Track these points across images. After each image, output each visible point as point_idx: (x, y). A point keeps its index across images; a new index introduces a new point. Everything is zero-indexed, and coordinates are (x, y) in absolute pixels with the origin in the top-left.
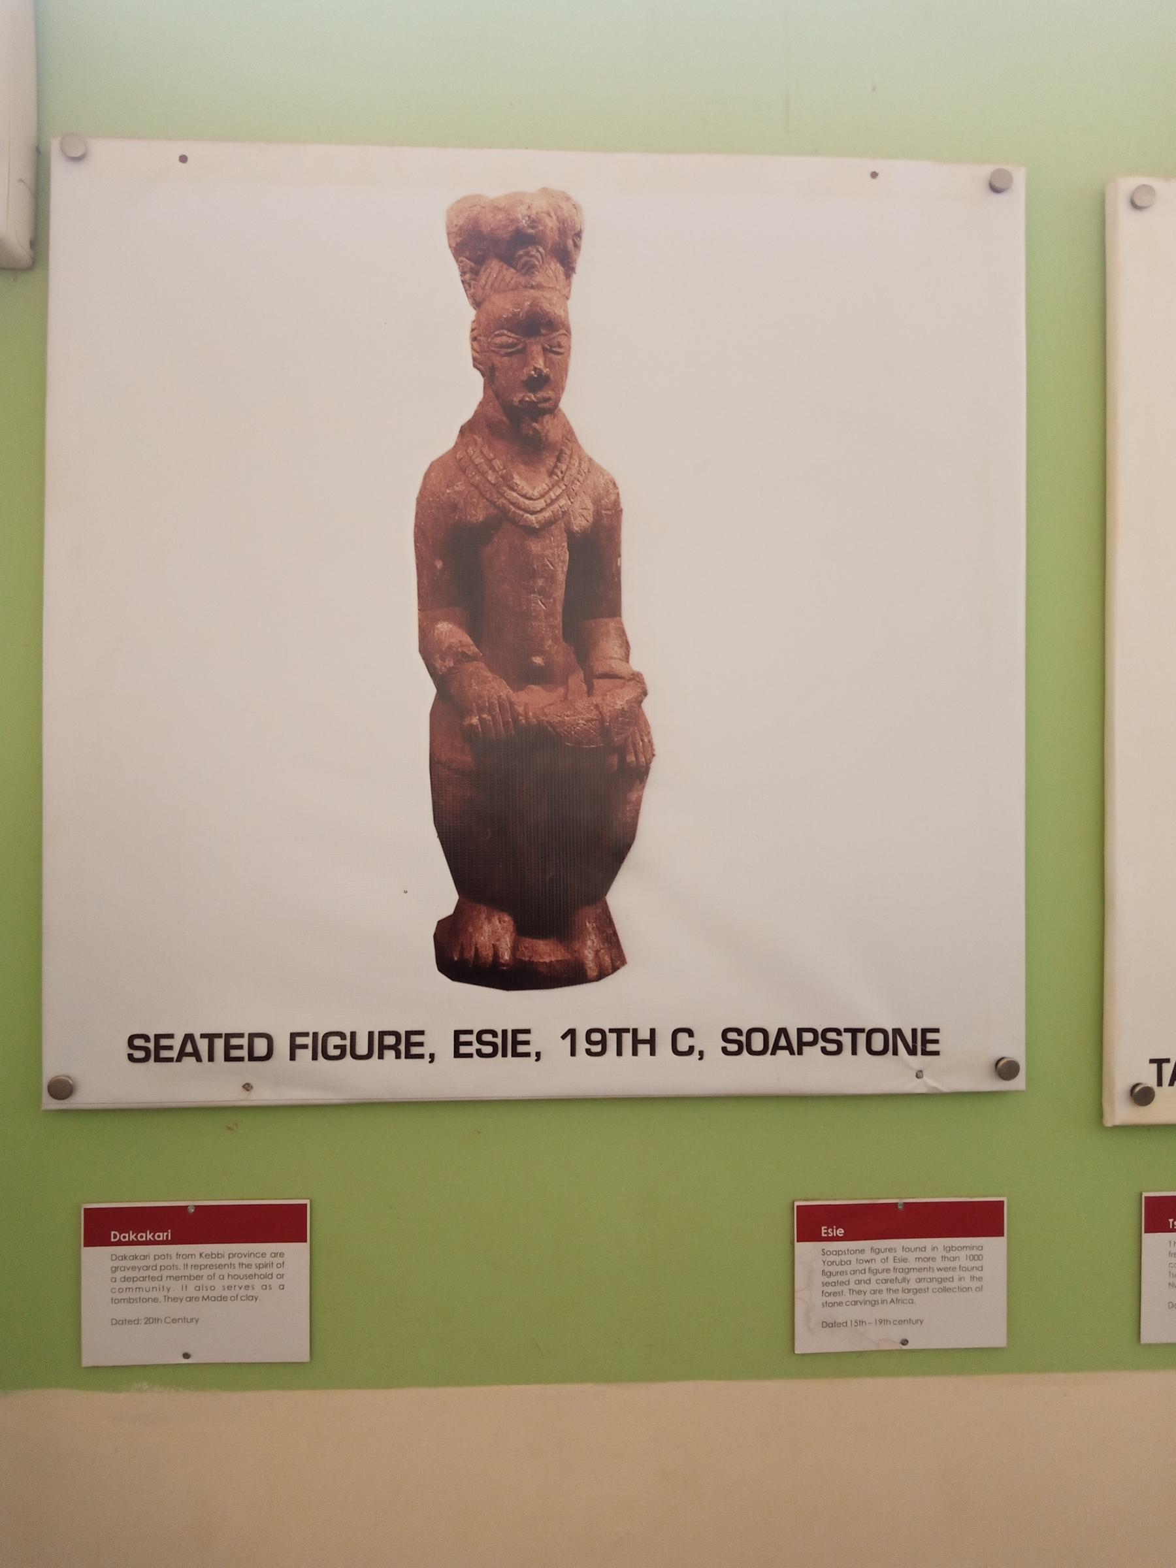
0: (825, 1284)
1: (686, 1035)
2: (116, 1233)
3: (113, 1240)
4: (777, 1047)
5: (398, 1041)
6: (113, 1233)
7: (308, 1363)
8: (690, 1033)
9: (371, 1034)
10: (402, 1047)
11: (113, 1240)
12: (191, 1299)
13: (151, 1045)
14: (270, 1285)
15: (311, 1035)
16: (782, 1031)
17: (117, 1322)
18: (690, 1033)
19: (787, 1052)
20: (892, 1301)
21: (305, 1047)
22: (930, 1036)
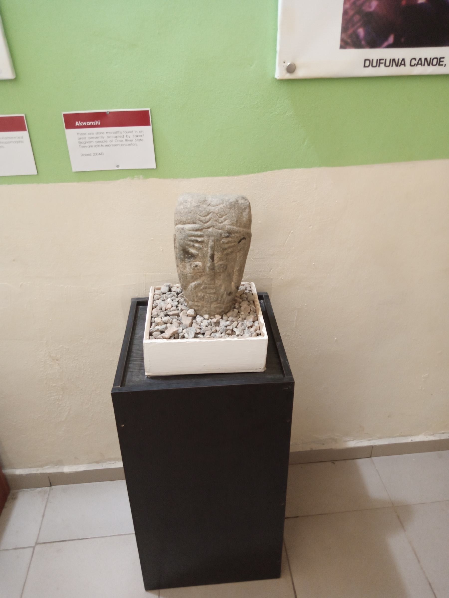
4: (401, 64)
7: (155, 169)
9: (377, 60)
12: (123, 145)
14: (142, 140)
15: (384, 60)
17: (82, 155)
21: (382, 63)
22: (442, 60)
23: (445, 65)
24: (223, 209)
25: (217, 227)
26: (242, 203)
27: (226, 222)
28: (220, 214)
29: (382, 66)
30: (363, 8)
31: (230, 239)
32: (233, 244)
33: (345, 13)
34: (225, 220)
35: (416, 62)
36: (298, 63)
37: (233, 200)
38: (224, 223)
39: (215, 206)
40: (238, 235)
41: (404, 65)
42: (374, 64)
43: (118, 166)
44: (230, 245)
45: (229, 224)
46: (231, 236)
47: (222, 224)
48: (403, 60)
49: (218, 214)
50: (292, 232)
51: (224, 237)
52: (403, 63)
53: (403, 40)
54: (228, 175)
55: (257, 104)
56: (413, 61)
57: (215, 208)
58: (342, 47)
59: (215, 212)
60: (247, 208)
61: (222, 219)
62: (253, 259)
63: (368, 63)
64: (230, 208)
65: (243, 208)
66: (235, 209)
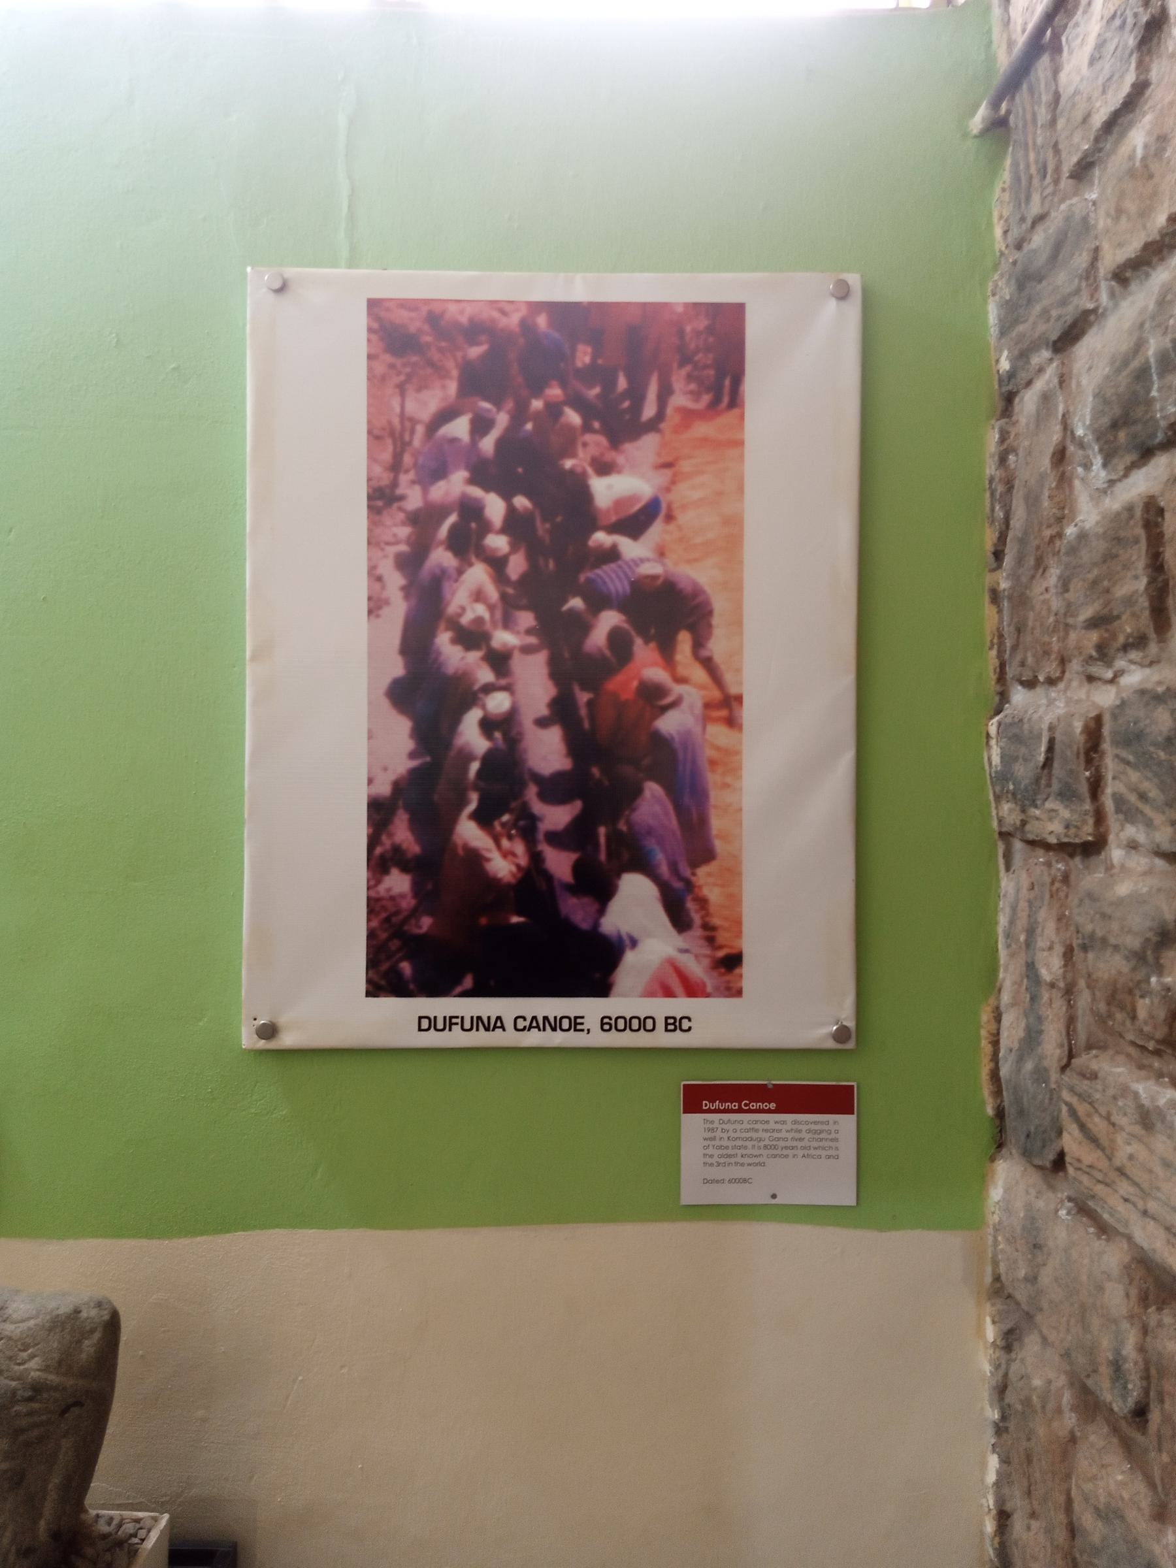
0: (836, 1140)
1: (687, 1020)
2: (707, 1102)
3: (704, 1108)
4: (495, 1027)
5: (675, 1021)
6: (704, 1102)
8: (689, 1019)
9: (445, 1018)
10: (677, 1024)
11: (704, 1108)
13: (613, 1022)
16: (534, 1018)
17: (706, 1181)
18: (689, 1019)
19: (537, 1030)
20: (804, 1156)
21: (457, 1024)
22: (579, 1021)
23: (588, 1030)
24: (32, 1332)
25: (10, 1374)
26: (88, 1318)
27: (33, 1364)
28: (22, 1341)
29: (456, 1029)
30: (406, 928)
31: (36, 1406)
32: (44, 1418)
33: (371, 935)
34: (32, 1357)
35: (527, 1023)
36: (282, 1020)
37: (65, 1308)
38: (26, 1366)
39: (19, 1322)
40: (57, 1395)
41: (503, 1027)
42: (440, 1025)
43: (774, 1196)
44: (36, 1419)
45: (38, 1368)
46: (39, 1397)
47: (22, 1367)
48: (499, 1018)
49: (19, 1343)
50: (300, 1378)
51: (20, 1398)
52: (499, 1024)
53: (492, 983)
54: (149, 1236)
55: (211, 1092)
56: (520, 1021)
57: (16, 1328)
58: (369, 994)
59: (14, 1337)
60: (98, 1329)
61: (24, 1355)
62: (206, 1445)
63: (427, 1024)
64: (50, 1330)
65: (88, 1328)
66: (62, 1331)
